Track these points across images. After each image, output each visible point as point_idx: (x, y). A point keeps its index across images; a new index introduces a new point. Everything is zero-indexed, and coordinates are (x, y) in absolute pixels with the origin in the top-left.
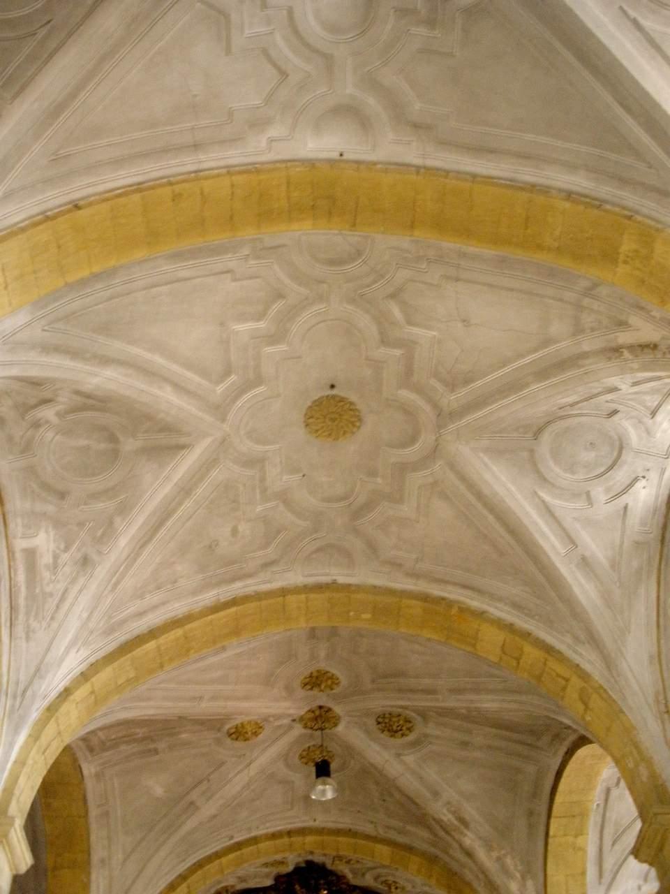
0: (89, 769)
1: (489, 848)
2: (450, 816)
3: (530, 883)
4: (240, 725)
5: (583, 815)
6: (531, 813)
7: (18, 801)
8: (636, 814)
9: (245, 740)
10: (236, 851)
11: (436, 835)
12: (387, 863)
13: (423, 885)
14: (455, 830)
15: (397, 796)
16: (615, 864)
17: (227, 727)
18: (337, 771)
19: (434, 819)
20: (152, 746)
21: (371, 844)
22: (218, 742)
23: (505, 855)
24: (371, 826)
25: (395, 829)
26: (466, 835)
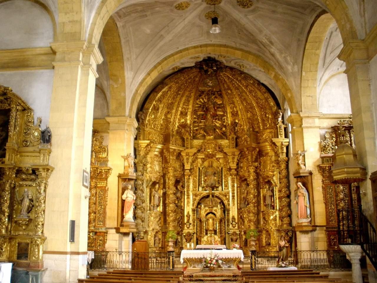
0: (119, 24)
1: (281, 52)
2: (266, 40)
4: (180, 3)
5: (320, 42)
6: (299, 40)
7: (95, 38)
8: (342, 42)
9: (182, 10)
10: (180, 53)
11: (260, 48)
12: (240, 58)
14: (268, 46)
15: (245, 32)
16: (330, 60)
17: (175, 5)
18: (220, 22)
19: (259, 41)
20: (144, 14)
22: (172, 11)
23: (287, 56)
24: (233, 43)
25: (243, 45)
26: (272, 48)
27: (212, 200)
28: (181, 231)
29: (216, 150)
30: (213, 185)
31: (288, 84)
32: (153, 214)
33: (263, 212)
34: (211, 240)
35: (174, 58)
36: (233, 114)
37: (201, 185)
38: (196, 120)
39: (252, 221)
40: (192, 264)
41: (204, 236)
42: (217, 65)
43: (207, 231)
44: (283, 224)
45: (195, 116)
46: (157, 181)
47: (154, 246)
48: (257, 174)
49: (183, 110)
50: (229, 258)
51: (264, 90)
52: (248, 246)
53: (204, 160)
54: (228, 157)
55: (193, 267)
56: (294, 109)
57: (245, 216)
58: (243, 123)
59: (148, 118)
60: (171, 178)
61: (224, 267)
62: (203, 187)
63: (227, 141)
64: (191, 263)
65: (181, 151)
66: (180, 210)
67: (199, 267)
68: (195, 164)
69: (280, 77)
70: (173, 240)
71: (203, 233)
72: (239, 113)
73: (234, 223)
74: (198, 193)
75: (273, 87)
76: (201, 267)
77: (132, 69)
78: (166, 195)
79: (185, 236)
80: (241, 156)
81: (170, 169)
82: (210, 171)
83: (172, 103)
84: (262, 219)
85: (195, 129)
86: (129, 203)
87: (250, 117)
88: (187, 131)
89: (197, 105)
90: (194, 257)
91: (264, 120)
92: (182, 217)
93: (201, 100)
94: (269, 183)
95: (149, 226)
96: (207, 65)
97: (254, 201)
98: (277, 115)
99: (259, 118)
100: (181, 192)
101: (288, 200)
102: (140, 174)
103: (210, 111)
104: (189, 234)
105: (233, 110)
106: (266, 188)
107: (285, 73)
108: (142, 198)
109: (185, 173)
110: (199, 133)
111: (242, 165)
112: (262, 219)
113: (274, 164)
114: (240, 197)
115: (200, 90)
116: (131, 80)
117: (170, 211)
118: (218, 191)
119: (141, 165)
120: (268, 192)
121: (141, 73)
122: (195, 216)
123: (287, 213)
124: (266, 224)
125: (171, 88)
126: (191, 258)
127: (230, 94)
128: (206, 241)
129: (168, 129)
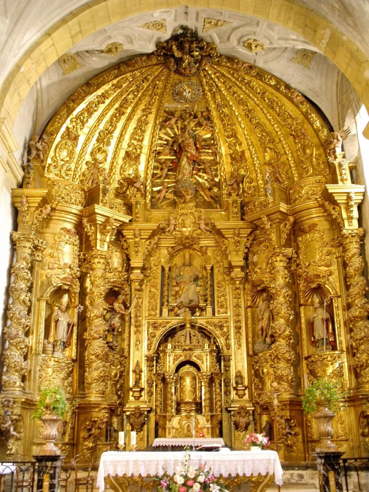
13: (279, 39)
27: (190, 334)
28: (120, 404)
29: (199, 228)
30: (193, 303)
31: (363, 51)
33: (306, 358)
34: (189, 426)
36: (233, 159)
37: (166, 303)
38: (158, 171)
39: (285, 378)
41: (173, 416)
42: (201, 49)
43: (178, 404)
49: (131, 149)
50: (241, 474)
54: (226, 241)
57: (265, 370)
58: (257, 174)
59: (52, 153)
60: (99, 281)
63: (223, 213)
65: (124, 223)
69: (344, 38)
71: (169, 408)
72: (247, 154)
73: (240, 387)
74: (161, 321)
78: (85, 323)
80: (253, 240)
82: (187, 273)
84: (305, 376)
85: (155, 189)
88: (138, 190)
89: (160, 142)
90: (136, 475)
92: (123, 375)
93: (168, 129)
94: (319, 290)
96: (181, 47)
97: (287, 332)
98: (331, 143)
99: (290, 158)
100: (122, 317)
102: (22, 266)
103: (186, 151)
104: (138, 413)
106: (312, 304)
110: (164, 197)
111: (255, 258)
112: (305, 376)
114: (253, 329)
115: (167, 109)
117: (93, 357)
118: (203, 316)
119: (28, 245)
120: (320, 311)
126: (129, 475)
127: (227, 115)
128: (177, 429)
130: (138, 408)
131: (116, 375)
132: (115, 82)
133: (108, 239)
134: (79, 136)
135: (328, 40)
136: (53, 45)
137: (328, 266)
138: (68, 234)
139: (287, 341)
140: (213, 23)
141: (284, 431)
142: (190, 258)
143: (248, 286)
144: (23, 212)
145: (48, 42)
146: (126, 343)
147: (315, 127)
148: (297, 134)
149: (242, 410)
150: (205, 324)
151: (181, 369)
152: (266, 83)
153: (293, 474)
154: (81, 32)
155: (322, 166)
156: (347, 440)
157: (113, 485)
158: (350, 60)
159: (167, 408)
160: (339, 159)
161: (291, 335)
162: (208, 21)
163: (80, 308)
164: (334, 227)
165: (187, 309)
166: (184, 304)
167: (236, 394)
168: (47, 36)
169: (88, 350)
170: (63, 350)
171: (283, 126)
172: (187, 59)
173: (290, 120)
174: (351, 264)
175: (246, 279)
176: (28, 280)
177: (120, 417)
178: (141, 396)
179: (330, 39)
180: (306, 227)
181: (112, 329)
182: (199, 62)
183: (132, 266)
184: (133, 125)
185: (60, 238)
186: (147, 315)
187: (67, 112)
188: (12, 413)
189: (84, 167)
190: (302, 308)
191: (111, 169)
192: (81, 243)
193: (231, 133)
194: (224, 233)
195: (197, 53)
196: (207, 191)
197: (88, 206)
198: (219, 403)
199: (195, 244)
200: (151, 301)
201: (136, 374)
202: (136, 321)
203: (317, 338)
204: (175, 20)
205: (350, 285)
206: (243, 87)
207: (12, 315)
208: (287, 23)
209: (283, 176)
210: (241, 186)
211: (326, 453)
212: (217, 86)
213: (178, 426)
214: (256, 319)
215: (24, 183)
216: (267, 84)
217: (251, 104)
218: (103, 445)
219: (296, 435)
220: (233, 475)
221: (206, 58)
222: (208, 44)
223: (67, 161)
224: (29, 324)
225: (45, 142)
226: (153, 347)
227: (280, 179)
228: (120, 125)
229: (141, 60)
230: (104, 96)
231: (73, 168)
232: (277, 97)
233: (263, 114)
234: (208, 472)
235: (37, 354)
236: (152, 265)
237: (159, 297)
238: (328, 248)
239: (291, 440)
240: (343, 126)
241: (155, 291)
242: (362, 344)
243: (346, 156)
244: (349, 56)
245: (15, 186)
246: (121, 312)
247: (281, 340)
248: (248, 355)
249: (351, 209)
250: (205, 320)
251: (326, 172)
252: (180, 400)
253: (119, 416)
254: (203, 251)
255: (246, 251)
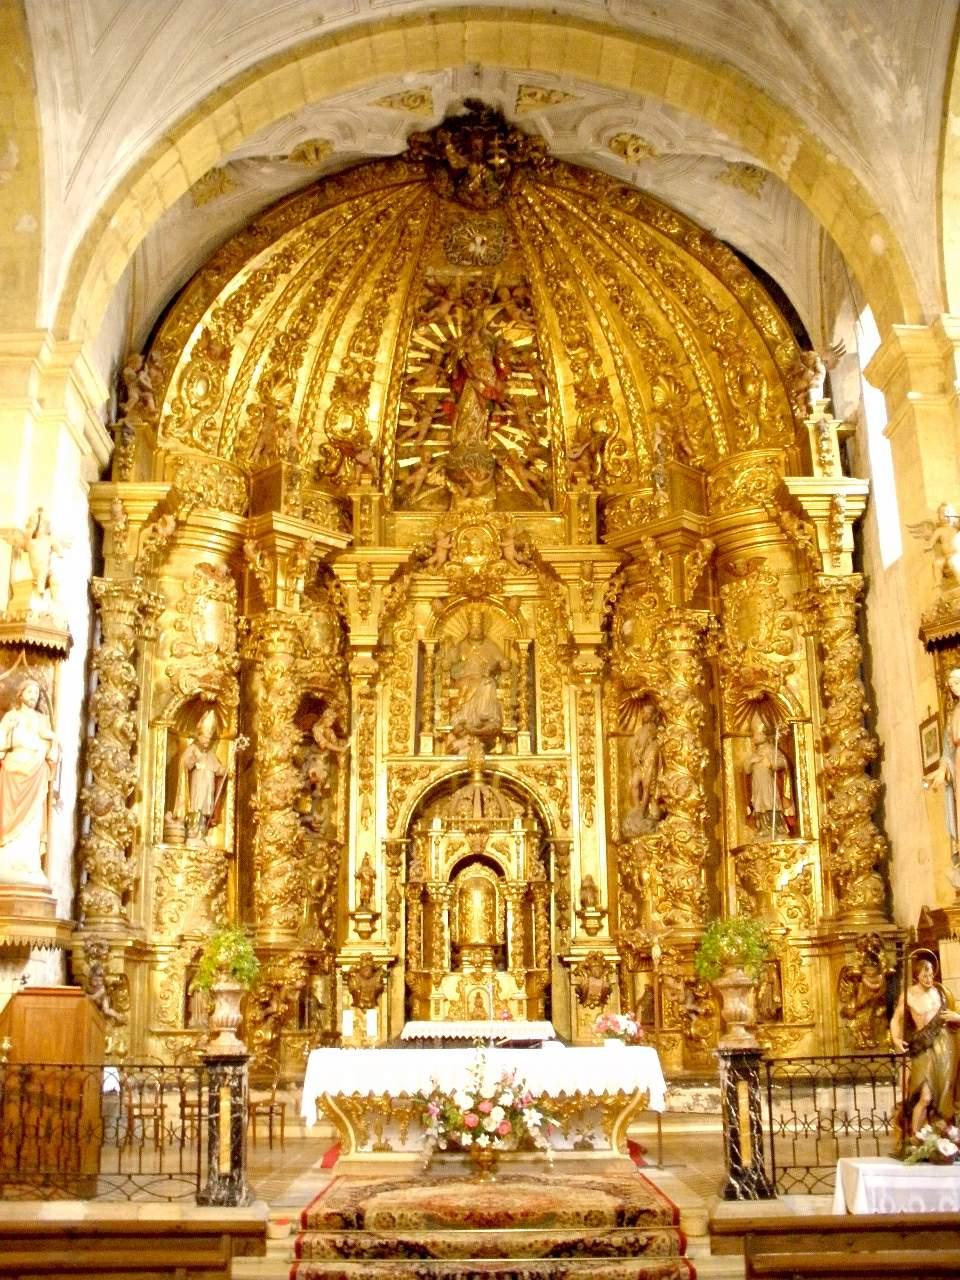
3: (913, 93)
13: (688, 138)
21: (596, 37)
23: (871, 37)
28: (330, 949)
29: (503, 557)
30: (489, 727)
32: (183, 863)
33: (735, 852)
34: (478, 996)
35: (300, 67)
36: (582, 396)
37: (428, 726)
38: (411, 423)
39: (686, 895)
40: (371, 1133)
41: (444, 975)
42: (511, 148)
43: (455, 949)
44: (850, 908)
45: (404, 406)
46: (211, 696)
47: (186, 1025)
48: (710, 674)
49: (348, 372)
50: (584, 1092)
51: (736, 267)
52: (666, 1027)
53: (444, 610)
54: (563, 589)
55: (377, 1149)
56: (904, 304)
57: (646, 876)
58: (634, 435)
59: (172, 392)
60: (280, 682)
61: (556, 1147)
62: (439, 740)
63: (558, 520)
64: (362, 1125)
65: (336, 551)
66: (323, 845)
67: (410, 1149)
68: (400, 628)
69: (830, 158)
70: (237, 987)
71: (436, 958)
72: (614, 387)
73: (590, 911)
74: (417, 765)
75: (776, 260)
76: (419, 1147)
77: (76, 100)
78: (253, 773)
79: (347, 976)
80: (623, 587)
81: (275, 635)
82: (475, 658)
83: (297, 337)
86: (19, 779)
87: (668, 401)
88: (366, 468)
89: (413, 354)
90: (379, 1093)
91: (737, 411)
92: (334, 885)
93: (434, 326)
94: (765, 704)
95: (159, 922)
96: (465, 148)
98: (801, 375)
99: (709, 402)
100: (332, 758)
101: (871, 786)
102: (117, 654)
103: (474, 378)
104: (370, 968)
105: (586, 377)
106: (751, 732)
107: (854, 136)
108: (122, 774)
109: (353, 667)
110: (424, 483)
111: (627, 627)
113: (791, 614)
114: (622, 784)
115: (431, 281)
116: (74, 156)
117: (272, 849)
118: (510, 754)
119: (129, 606)
120: (766, 750)
121: (127, 130)
122: (402, 878)
123: (867, 851)
124: (755, 913)
125: (288, 257)
126: (364, 1093)
127: (570, 298)
129: (272, 454)
130: (369, 957)
131: (319, 886)
132: (313, 222)
133: (301, 586)
134: (231, 349)
135: (794, 158)
136: (180, 161)
137: (786, 653)
138: (212, 577)
139: (692, 815)
140: (539, 96)
141: (681, 1008)
142: (482, 624)
143: (611, 689)
144: (115, 533)
145: (170, 157)
146: (340, 814)
147: (768, 336)
148: (726, 349)
149: (596, 962)
150: (515, 772)
151: (463, 872)
152: (658, 230)
153: (698, 1095)
154: (240, 127)
155: (780, 426)
156: (812, 1026)
157: (333, 1111)
158: (842, 207)
159: (431, 956)
160: (818, 414)
161: (701, 802)
162: (526, 91)
163: (242, 742)
164: (802, 566)
165: (476, 741)
166: (468, 726)
167: (583, 926)
168: (167, 145)
169: (259, 831)
170: (205, 834)
171: (694, 328)
172: (478, 172)
173: (711, 316)
174: (834, 652)
175: (606, 673)
176: (130, 685)
177: (328, 977)
178: (374, 930)
179: (799, 158)
180: (740, 562)
181: (310, 787)
182: (505, 177)
183: (352, 643)
184: (353, 318)
185: (195, 586)
186: (386, 751)
187: (205, 295)
188: (107, 970)
189: (244, 418)
190: (728, 743)
191: (304, 420)
192: (240, 595)
193: (577, 337)
194: (558, 571)
195: (502, 161)
196: (521, 468)
197: (255, 513)
198: (544, 948)
199: (495, 592)
200: (394, 720)
201: (363, 882)
202: (363, 765)
203: (757, 809)
204: (453, 86)
205: (830, 698)
206: (607, 236)
207: (98, 762)
208: (706, 111)
209: (694, 441)
210: (599, 459)
211: (734, 1050)
212: (547, 231)
213: (456, 997)
214: (627, 762)
215: (115, 465)
216: (662, 232)
217: (623, 272)
218: (293, 1035)
219: (707, 1015)
220: (570, 1093)
221: (522, 171)
222: (526, 137)
223: (207, 407)
224: (135, 781)
225: (157, 368)
226: (398, 823)
227: (687, 449)
228: (324, 318)
229: (374, 173)
230: (288, 256)
231: (219, 425)
232: (683, 263)
233: (650, 299)
234: (520, 1088)
235: (152, 844)
236: (398, 639)
237: (413, 710)
238: (789, 613)
239: (696, 1025)
240: (831, 340)
241: (404, 696)
242: (851, 826)
243: (837, 406)
244: (839, 197)
245: (96, 477)
246: (330, 746)
247: (679, 812)
248: (609, 840)
249: (839, 531)
250: (516, 764)
251: (788, 439)
252: (461, 940)
253: (326, 973)
254: (512, 606)
255: (607, 610)
